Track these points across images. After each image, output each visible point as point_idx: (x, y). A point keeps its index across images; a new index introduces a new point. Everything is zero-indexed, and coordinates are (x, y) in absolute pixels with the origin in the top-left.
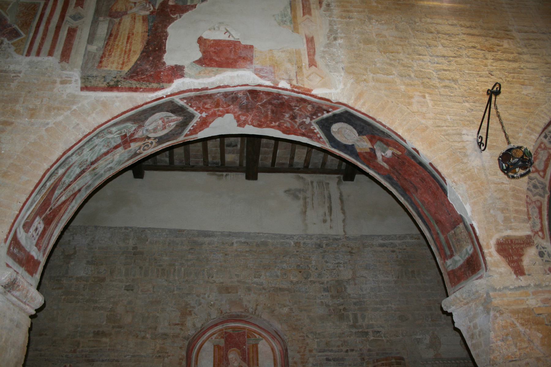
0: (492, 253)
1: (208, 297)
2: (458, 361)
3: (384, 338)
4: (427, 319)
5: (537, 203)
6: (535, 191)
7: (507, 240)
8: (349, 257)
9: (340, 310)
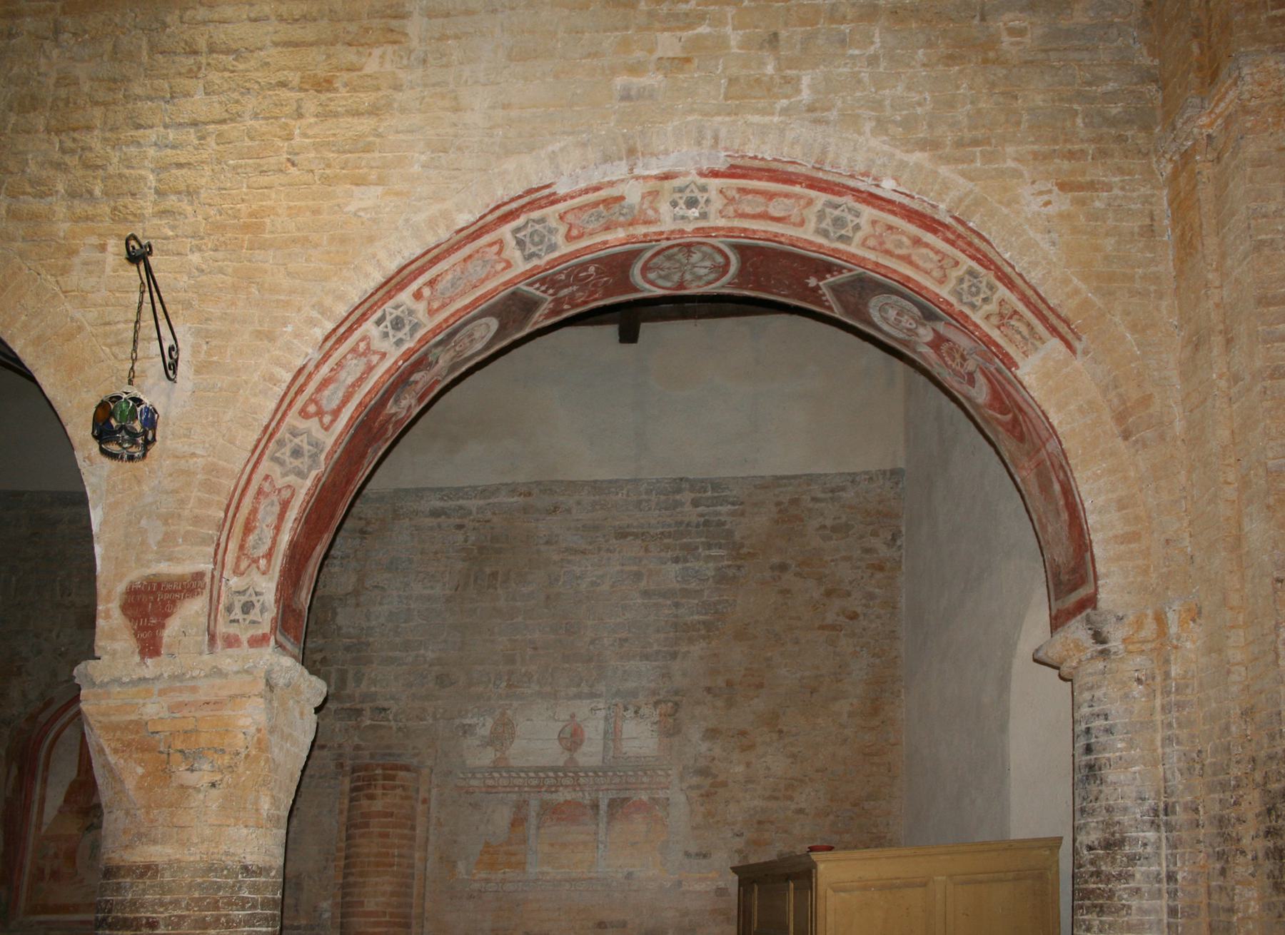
0: (111, 613)
1: (58, 636)
2: (542, 775)
3: (392, 723)
4: (498, 682)
5: (283, 492)
6: (291, 463)
7: (150, 583)
8: (358, 541)
9: (315, 662)
